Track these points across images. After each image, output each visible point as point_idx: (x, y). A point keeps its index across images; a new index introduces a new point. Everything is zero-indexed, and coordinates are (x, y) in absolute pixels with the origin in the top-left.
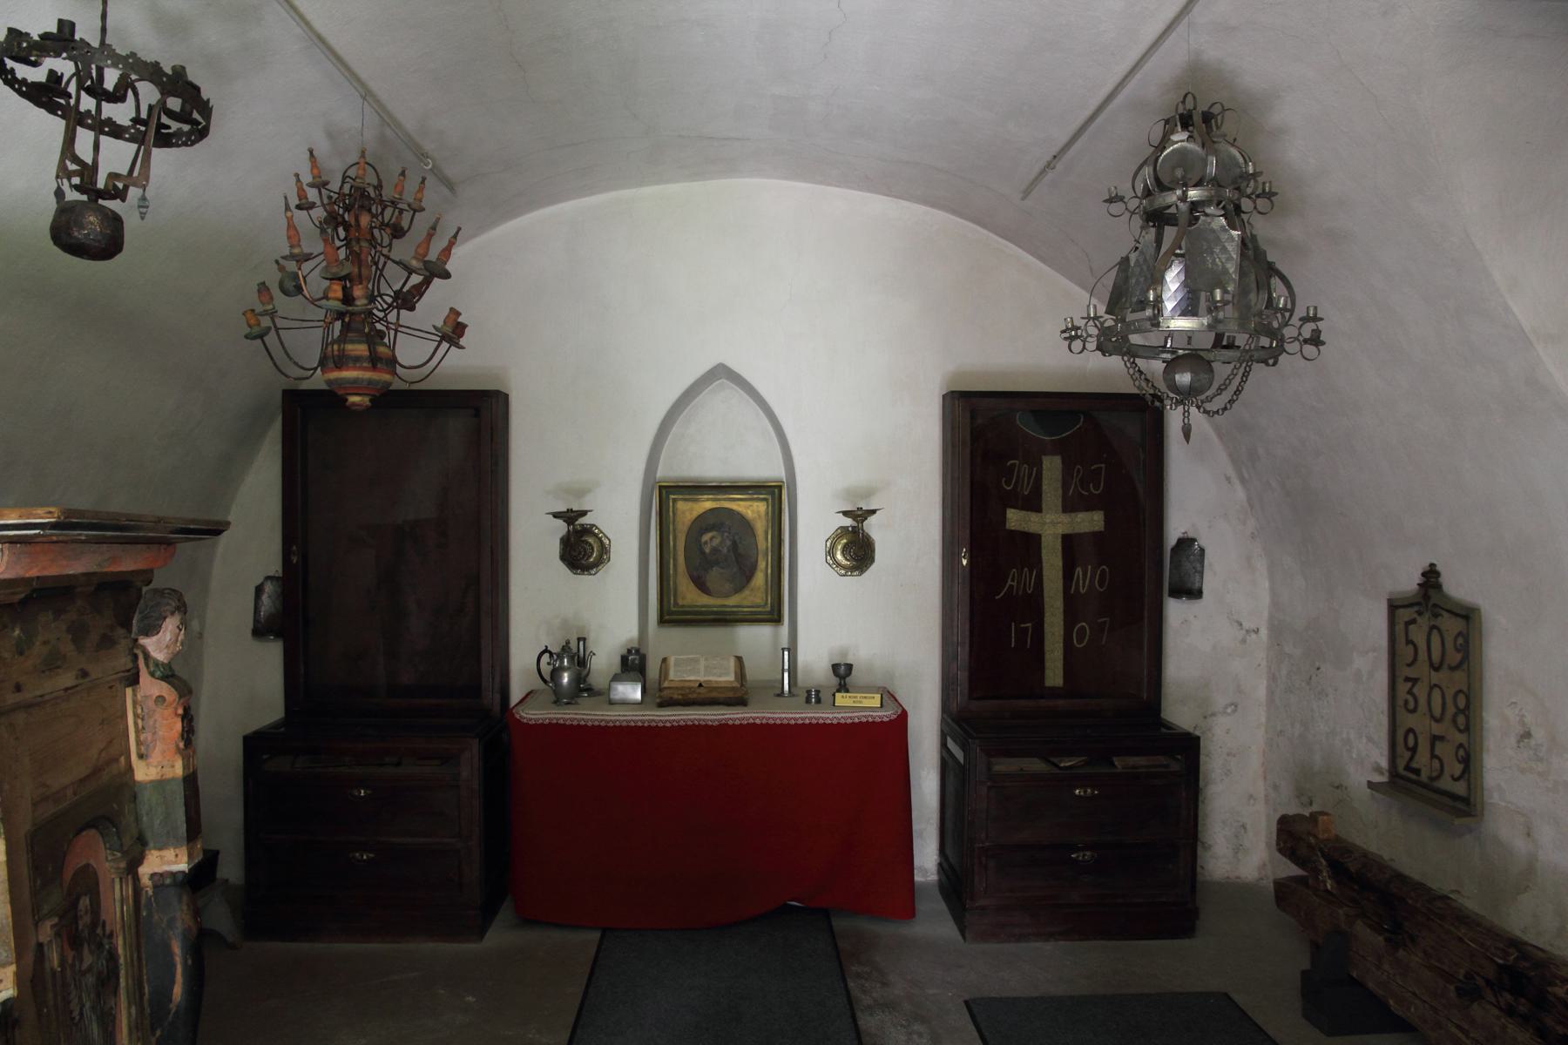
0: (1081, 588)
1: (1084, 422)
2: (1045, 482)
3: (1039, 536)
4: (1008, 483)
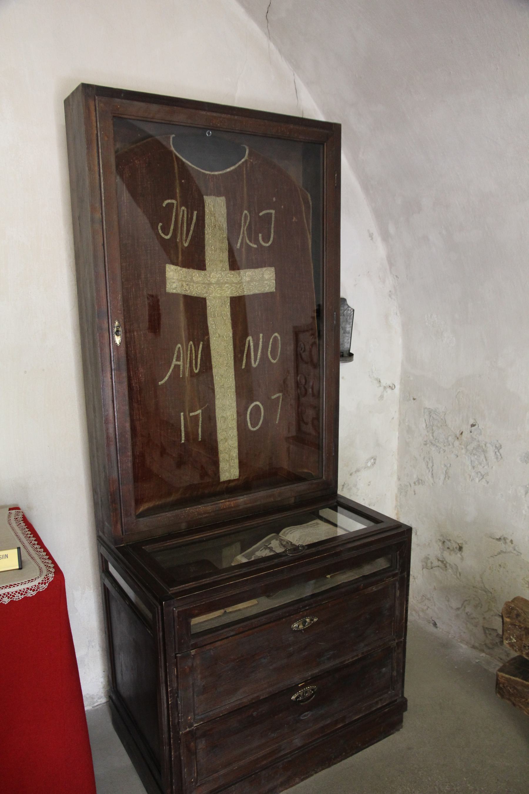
0: (253, 362)
1: (250, 154)
2: (208, 231)
3: (204, 299)
4: (166, 230)
